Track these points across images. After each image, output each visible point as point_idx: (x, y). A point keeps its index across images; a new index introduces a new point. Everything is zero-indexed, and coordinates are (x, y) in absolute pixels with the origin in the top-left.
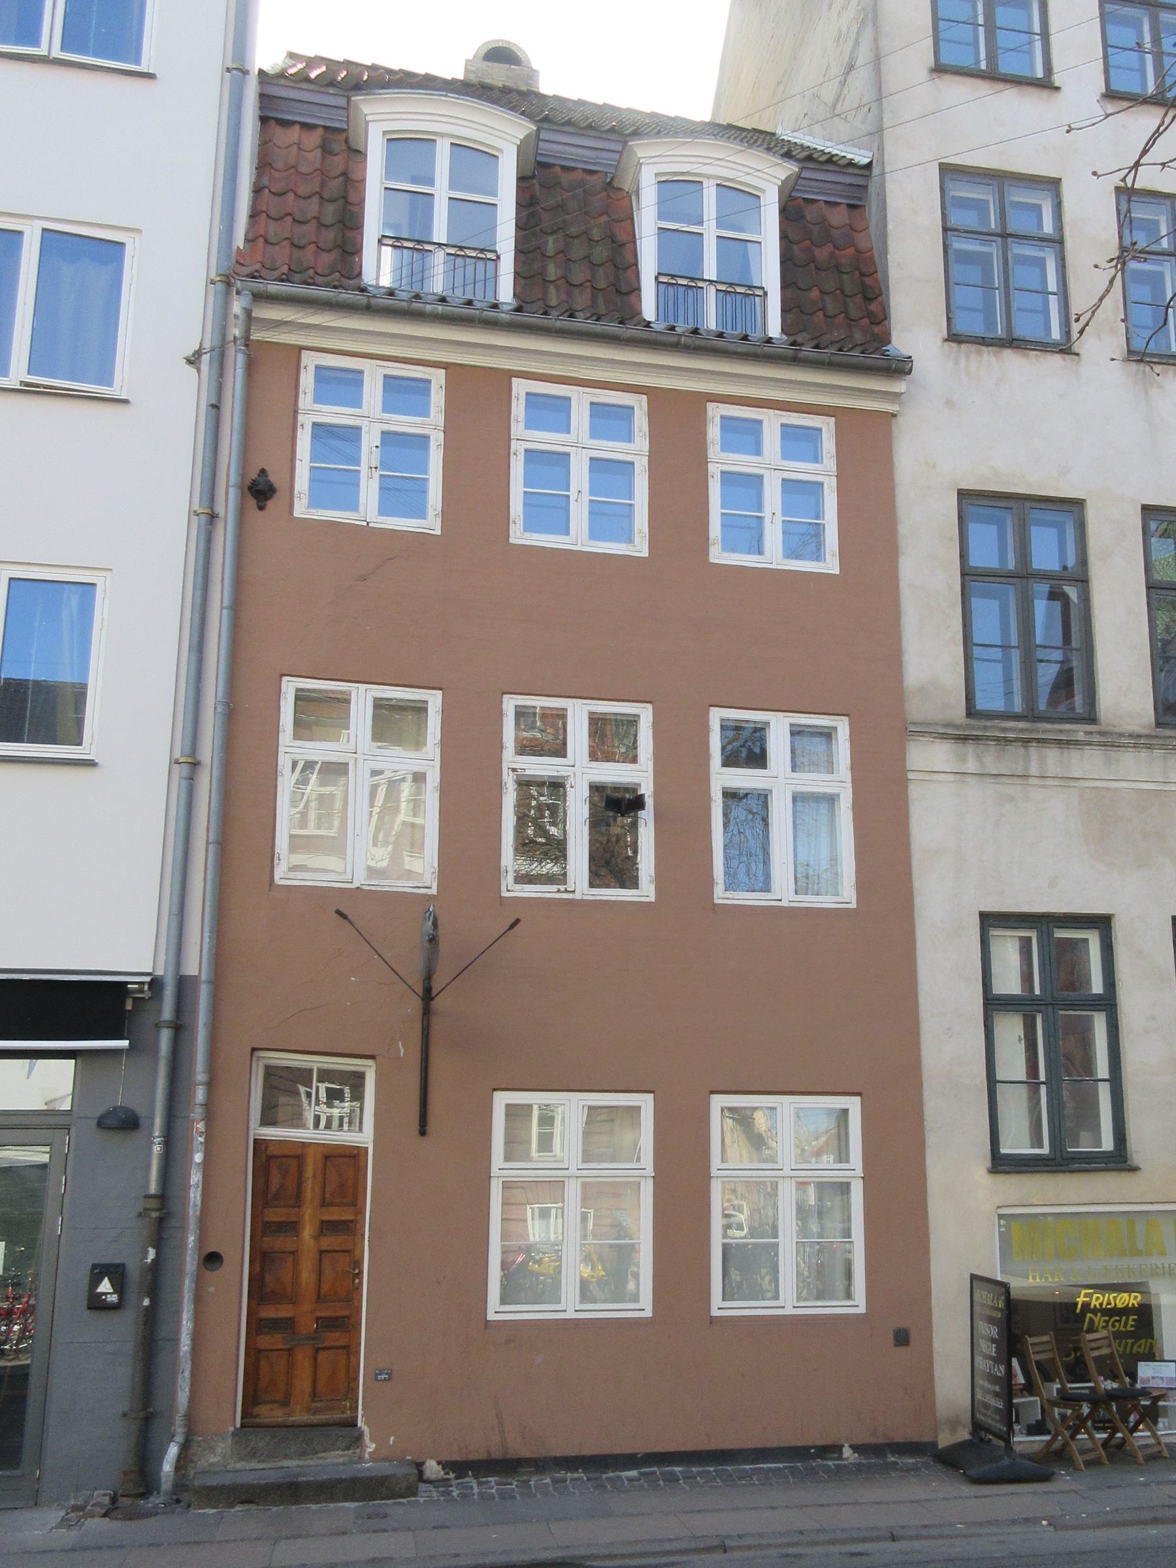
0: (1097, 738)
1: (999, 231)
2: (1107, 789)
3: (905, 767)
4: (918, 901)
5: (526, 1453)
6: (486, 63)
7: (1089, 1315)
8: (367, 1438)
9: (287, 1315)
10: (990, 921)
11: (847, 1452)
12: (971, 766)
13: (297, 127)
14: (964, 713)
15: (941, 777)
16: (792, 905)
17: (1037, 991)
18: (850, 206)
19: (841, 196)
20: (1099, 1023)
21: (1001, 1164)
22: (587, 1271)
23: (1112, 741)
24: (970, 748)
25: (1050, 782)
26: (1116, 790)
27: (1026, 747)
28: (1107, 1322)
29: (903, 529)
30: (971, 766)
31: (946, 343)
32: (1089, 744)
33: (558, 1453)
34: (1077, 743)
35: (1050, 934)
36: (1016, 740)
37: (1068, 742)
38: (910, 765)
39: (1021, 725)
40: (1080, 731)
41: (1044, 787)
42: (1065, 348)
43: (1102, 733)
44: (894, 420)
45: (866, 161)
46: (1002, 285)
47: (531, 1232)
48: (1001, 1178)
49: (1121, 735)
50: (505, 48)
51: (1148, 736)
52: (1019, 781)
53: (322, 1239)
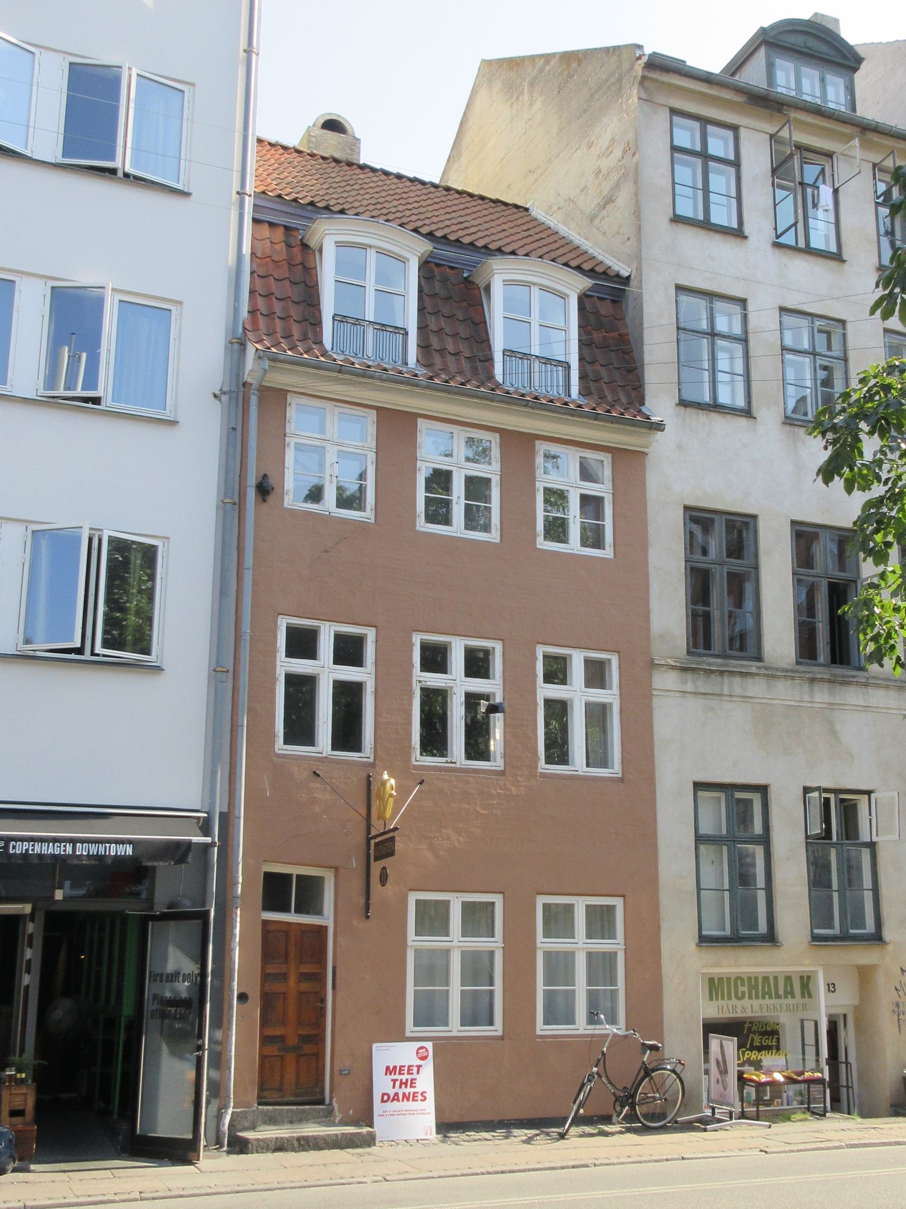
0: (763, 671)
1: (709, 331)
3: (651, 686)
7: (751, 1035)
8: (336, 1112)
9: (279, 1033)
10: (699, 786)
12: (689, 687)
13: (267, 225)
14: (686, 653)
15: (672, 694)
16: (584, 774)
18: (613, 301)
19: (606, 294)
20: (759, 851)
23: (772, 674)
24: (689, 676)
25: (735, 699)
26: (773, 705)
27: (722, 676)
28: (761, 1039)
29: (651, 530)
30: (689, 687)
31: (678, 408)
32: (758, 675)
35: (732, 796)
38: (654, 686)
39: (719, 661)
40: (753, 667)
42: (747, 413)
43: (766, 668)
45: (627, 274)
46: (711, 367)
49: (777, 669)
50: (336, 120)
51: (793, 671)
53: (301, 984)
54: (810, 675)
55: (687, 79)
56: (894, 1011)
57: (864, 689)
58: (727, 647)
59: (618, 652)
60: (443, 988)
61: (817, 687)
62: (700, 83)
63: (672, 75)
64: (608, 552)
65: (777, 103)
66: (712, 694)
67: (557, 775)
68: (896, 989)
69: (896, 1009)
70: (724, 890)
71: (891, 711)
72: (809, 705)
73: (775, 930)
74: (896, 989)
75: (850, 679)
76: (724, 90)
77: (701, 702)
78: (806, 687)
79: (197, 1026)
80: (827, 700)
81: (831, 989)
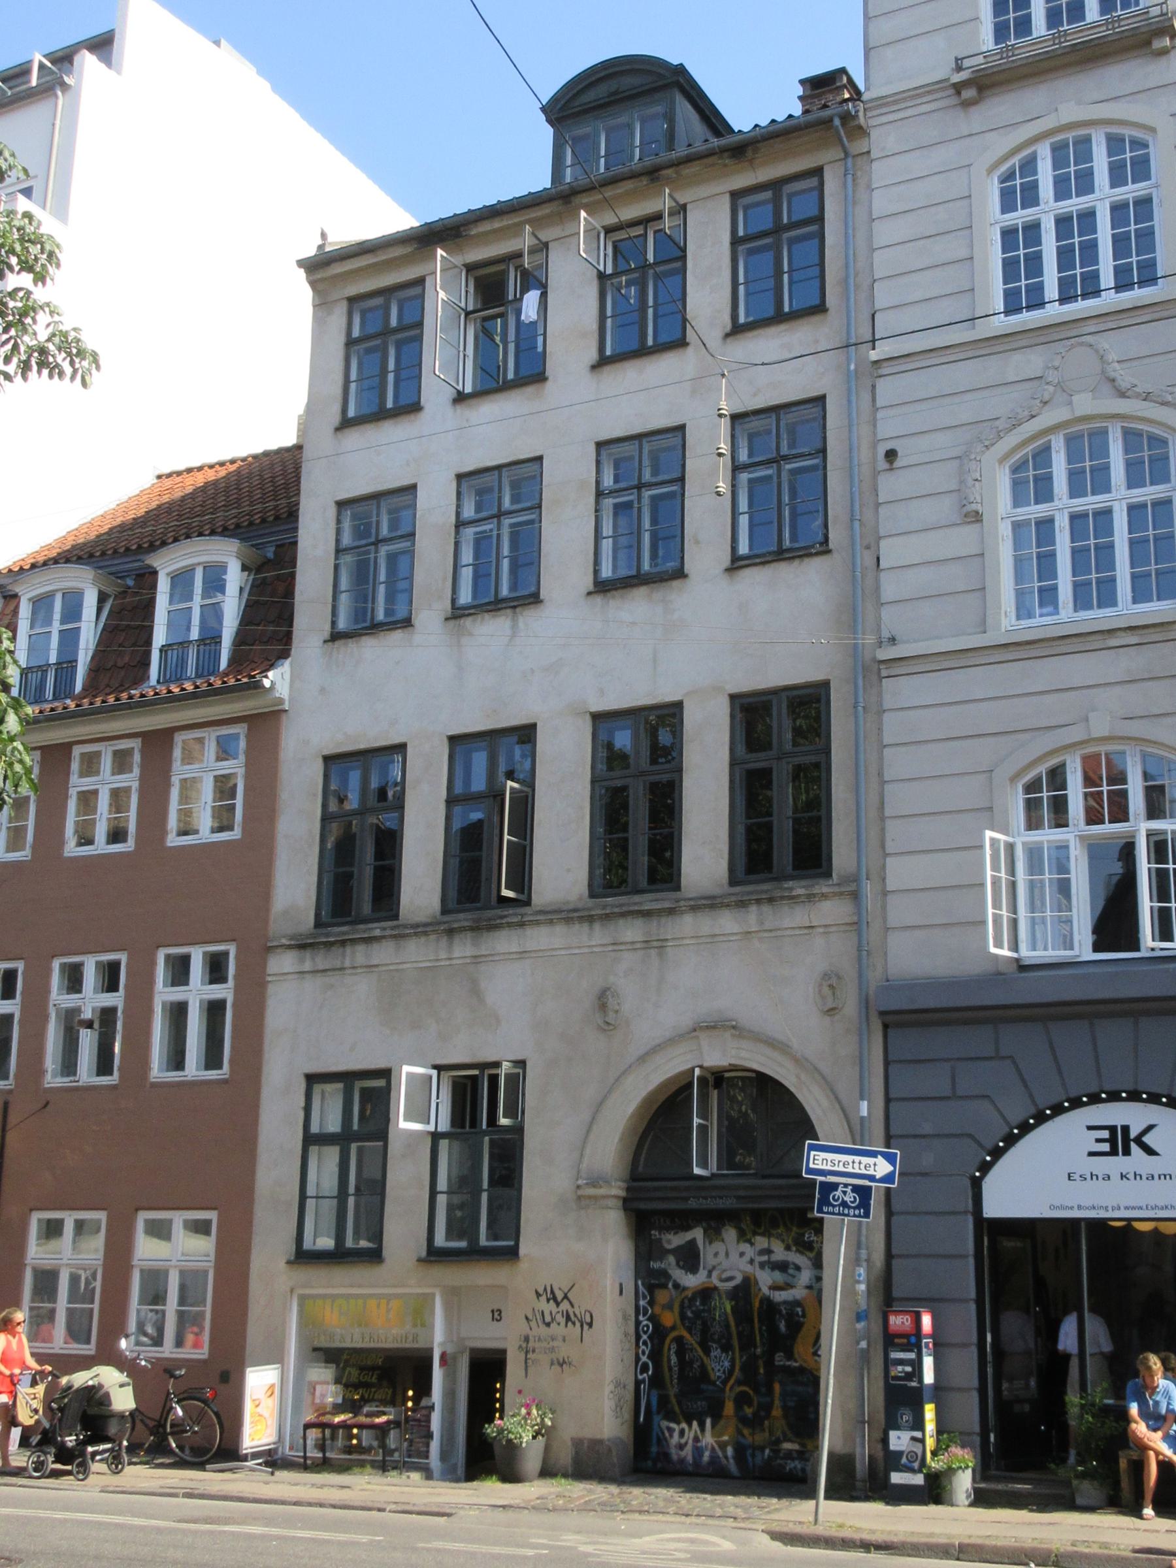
2: (397, 970)
10: (312, 1079)
15: (290, 977)
17: (355, 1127)
22: (769, 793)
24: (308, 954)
25: (359, 970)
30: (307, 966)
37: (370, 938)
47: (791, 824)
54: (446, 926)
55: (348, 261)
56: (520, 1347)
57: (519, 931)
60: (85, 1306)
61: (457, 939)
62: (359, 258)
63: (333, 266)
65: (451, 229)
66: (334, 970)
67: (167, 1083)
68: (527, 1318)
69: (524, 1345)
70: (317, 1197)
73: (633, 1249)
74: (527, 1318)
75: (498, 921)
76: (391, 250)
77: (320, 980)
78: (444, 941)
79: (830, 1401)
80: (468, 954)
81: (496, 1314)
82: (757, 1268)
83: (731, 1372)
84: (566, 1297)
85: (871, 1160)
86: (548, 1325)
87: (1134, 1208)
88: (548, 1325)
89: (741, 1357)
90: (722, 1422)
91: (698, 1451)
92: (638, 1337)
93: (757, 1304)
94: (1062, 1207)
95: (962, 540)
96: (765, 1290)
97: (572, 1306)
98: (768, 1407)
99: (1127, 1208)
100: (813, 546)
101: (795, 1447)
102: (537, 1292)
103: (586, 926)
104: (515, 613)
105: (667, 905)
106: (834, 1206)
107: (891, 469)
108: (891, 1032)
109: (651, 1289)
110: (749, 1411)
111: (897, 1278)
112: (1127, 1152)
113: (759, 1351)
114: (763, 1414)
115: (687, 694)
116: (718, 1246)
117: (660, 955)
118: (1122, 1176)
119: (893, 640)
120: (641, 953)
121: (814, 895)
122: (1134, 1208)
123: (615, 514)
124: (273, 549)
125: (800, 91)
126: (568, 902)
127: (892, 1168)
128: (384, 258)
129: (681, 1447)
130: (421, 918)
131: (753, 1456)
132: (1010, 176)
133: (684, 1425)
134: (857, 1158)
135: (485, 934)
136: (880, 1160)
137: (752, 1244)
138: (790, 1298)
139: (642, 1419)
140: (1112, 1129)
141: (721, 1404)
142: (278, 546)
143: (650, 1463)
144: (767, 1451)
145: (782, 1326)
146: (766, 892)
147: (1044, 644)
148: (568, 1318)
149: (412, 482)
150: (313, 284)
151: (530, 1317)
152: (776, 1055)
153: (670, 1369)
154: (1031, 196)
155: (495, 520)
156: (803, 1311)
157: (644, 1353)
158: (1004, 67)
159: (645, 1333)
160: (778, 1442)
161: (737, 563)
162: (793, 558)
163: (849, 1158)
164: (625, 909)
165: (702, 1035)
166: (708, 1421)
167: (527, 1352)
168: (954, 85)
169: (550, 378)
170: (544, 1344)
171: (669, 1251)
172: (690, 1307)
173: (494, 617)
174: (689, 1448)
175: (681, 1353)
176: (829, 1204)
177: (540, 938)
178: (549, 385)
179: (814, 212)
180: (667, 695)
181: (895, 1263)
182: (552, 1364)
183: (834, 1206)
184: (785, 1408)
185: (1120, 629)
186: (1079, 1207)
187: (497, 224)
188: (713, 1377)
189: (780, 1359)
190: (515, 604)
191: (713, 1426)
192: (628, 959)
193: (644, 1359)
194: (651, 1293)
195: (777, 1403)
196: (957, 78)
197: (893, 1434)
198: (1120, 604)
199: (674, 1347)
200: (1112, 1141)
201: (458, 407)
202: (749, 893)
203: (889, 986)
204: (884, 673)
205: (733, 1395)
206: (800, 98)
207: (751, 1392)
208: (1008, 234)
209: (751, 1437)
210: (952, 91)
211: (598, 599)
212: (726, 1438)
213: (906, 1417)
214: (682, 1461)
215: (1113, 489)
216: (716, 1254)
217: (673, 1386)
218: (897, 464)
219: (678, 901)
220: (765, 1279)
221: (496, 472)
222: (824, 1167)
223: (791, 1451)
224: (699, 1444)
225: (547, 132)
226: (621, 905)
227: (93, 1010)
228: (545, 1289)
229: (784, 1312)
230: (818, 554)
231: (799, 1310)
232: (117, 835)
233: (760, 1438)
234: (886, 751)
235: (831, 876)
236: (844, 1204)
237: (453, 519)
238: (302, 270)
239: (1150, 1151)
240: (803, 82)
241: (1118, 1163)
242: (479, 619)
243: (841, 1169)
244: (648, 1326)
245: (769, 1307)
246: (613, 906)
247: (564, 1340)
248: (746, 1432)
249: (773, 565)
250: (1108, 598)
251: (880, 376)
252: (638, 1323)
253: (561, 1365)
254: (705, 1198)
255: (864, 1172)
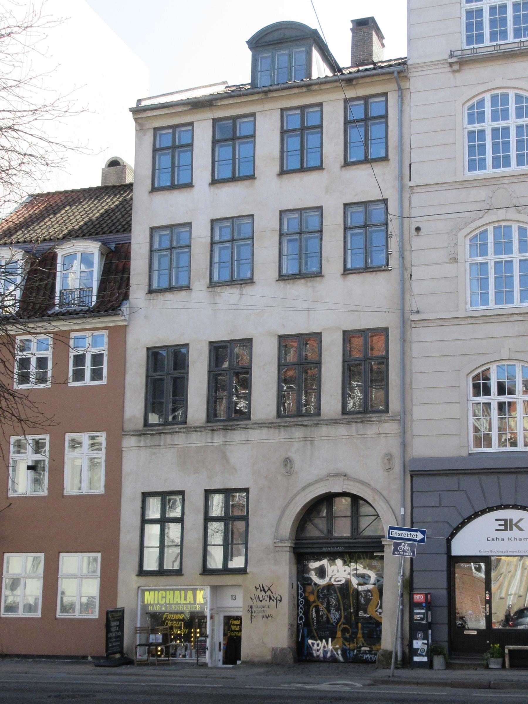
2: (187, 447)
4: (123, 491)
5: (7, 653)
6: (109, 168)
7: (167, 621)
11: (89, 658)
21: (142, 572)
23: (190, 430)
24: (142, 438)
25: (168, 447)
26: (190, 447)
32: (180, 432)
33: (15, 653)
34: (176, 432)
36: (156, 433)
37: (173, 432)
38: (123, 446)
41: (166, 448)
44: (127, 327)
48: (140, 578)
52: (157, 447)
54: (211, 428)
57: (245, 431)
58: (474, 402)
59: (65, 433)
61: (216, 433)
64: (104, 382)
68: (251, 598)
69: (250, 610)
71: (264, 441)
72: (211, 444)
74: (251, 598)
78: (210, 433)
81: (233, 597)
82: (352, 576)
83: (340, 619)
84: (269, 589)
85: (415, 533)
86: (261, 601)
87: (513, 552)
88: (261, 601)
89: (344, 613)
90: (336, 640)
91: (325, 652)
92: (298, 606)
93: (351, 592)
94: (484, 551)
95: (450, 269)
96: (356, 586)
97: (272, 593)
98: (356, 633)
99: (510, 552)
100: (381, 267)
101: (368, 649)
102: (256, 587)
103: (277, 430)
104: (241, 287)
105: (315, 422)
106: (400, 552)
107: (418, 236)
108: (415, 479)
109: (304, 585)
110: (348, 635)
111: (415, 580)
112: (511, 530)
113: (352, 611)
114: (354, 636)
115: (324, 329)
116: (334, 567)
117: (311, 444)
118: (509, 539)
119: (418, 312)
120: (302, 443)
121: (381, 421)
122: (513, 552)
123: (288, 243)
124: (114, 245)
125: (351, 26)
126: (268, 419)
127: (423, 536)
128: (173, 111)
129: (318, 650)
130: (198, 424)
131: (350, 653)
132: (472, 107)
133: (319, 642)
134: (409, 533)
135: (229, 432)
136: (419, 533)
137: (349, 567)
138: (366, 589)
139: (300, 640)
140: (506, 520)
141: (336, 633)
142: (116, 244)
143: (304, 658)
144: (355, 651)
145: (362, 601)
146: (360, 418)
147: (483, 318)
148: (270, 598)
149: (189, 221)
150: (136, 120)
151: (253, 598)
152: (364, 488)
153: (313, 618)
154: (481, 118)
155: (231, 243)
156: (371, 594)
157: (301, 612)
158: (471, 58)
159: (301, 604)
160: (360, 647)
161: (346, 272)
162: (373, 271)
163: (406, 532)
164: (295, 423)
165: (331, 479)
166: (330, 640)
167: (252, 613)
168: (450, 63)
169: (258, 178)
170: (259, 609)
171: (312, 570)
172: (322, 593)
173: (231, 288)
174: (321, 651)
175: (317, 612)
176: (398, 551)
177: (255, 434)
178: (257, 182)
179: (383, 113)
180: (314, 329)
181: (415, 574)
182: (263, 617)
183: (400, 552)
184: (363, 634)
185: (515, 314)
186: (491, 551)
187: (231, 101)
188: (332, 622)
189: (361, 614)
190: (242, 282)
191: (332, 641)
192: (297, 445)
193: (301, 615)
194: (304, 587)
195: (360, 631)
196: (451, 60)
197: (415, 642)
198: (515, 302)
199: (314, 609)
200: (505, 525)
201: (212, 187)
202: (353, 418)
203: (414, 460)
204: (413, 326)
205: (341, 628)
206: (351, 29)
207: (349, 628)
208: (471, 134)
209: (348, 646)
210: (448, 65)
211: (281, 283)
212: (337, 646)
213: (421, 635)
214: (318, 656)
215: (514, 253)
216: (333, 571)
217: (314, 626)
218: (420, 233)
219: (320, 421)
220: (355, 581)
221: (231, 220)
222: (396, 536)
223: (365, 651)
224: (326, 649)
225: (249, 54)
226: (293, 422)
227: (32, 461)
228: (260, 586)
229: (363, 595)
230: (384, 270)
231: (370, 593)
232: (42, 379)
233: (352, 646)
234: (413, 360)
235: (388, 412)
236: (404, 551)
237: (208, 240)
238: (131, 113)
239: (520, 529)
240: (353, 21)
241: (508, 534)
242: (224, 289)
243: (403, 537)
244: (302, 601)
245: (357, 593)
246: (290, 422)
247: (269, 607)
248: (346, 643)
249: (364, 274)
250: (510, 300)
251: (413, 193)
252: (298, 600)
253: (267, 618)
254: (330, 547)
255: (412, 538)
